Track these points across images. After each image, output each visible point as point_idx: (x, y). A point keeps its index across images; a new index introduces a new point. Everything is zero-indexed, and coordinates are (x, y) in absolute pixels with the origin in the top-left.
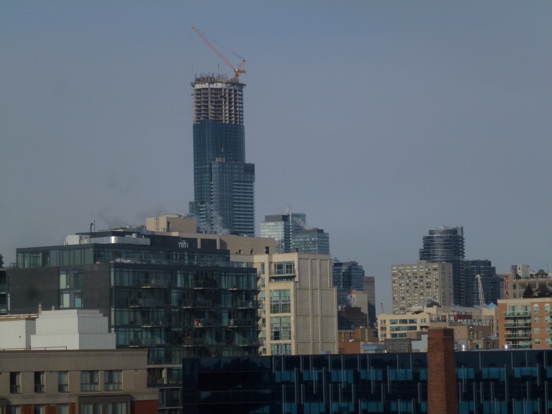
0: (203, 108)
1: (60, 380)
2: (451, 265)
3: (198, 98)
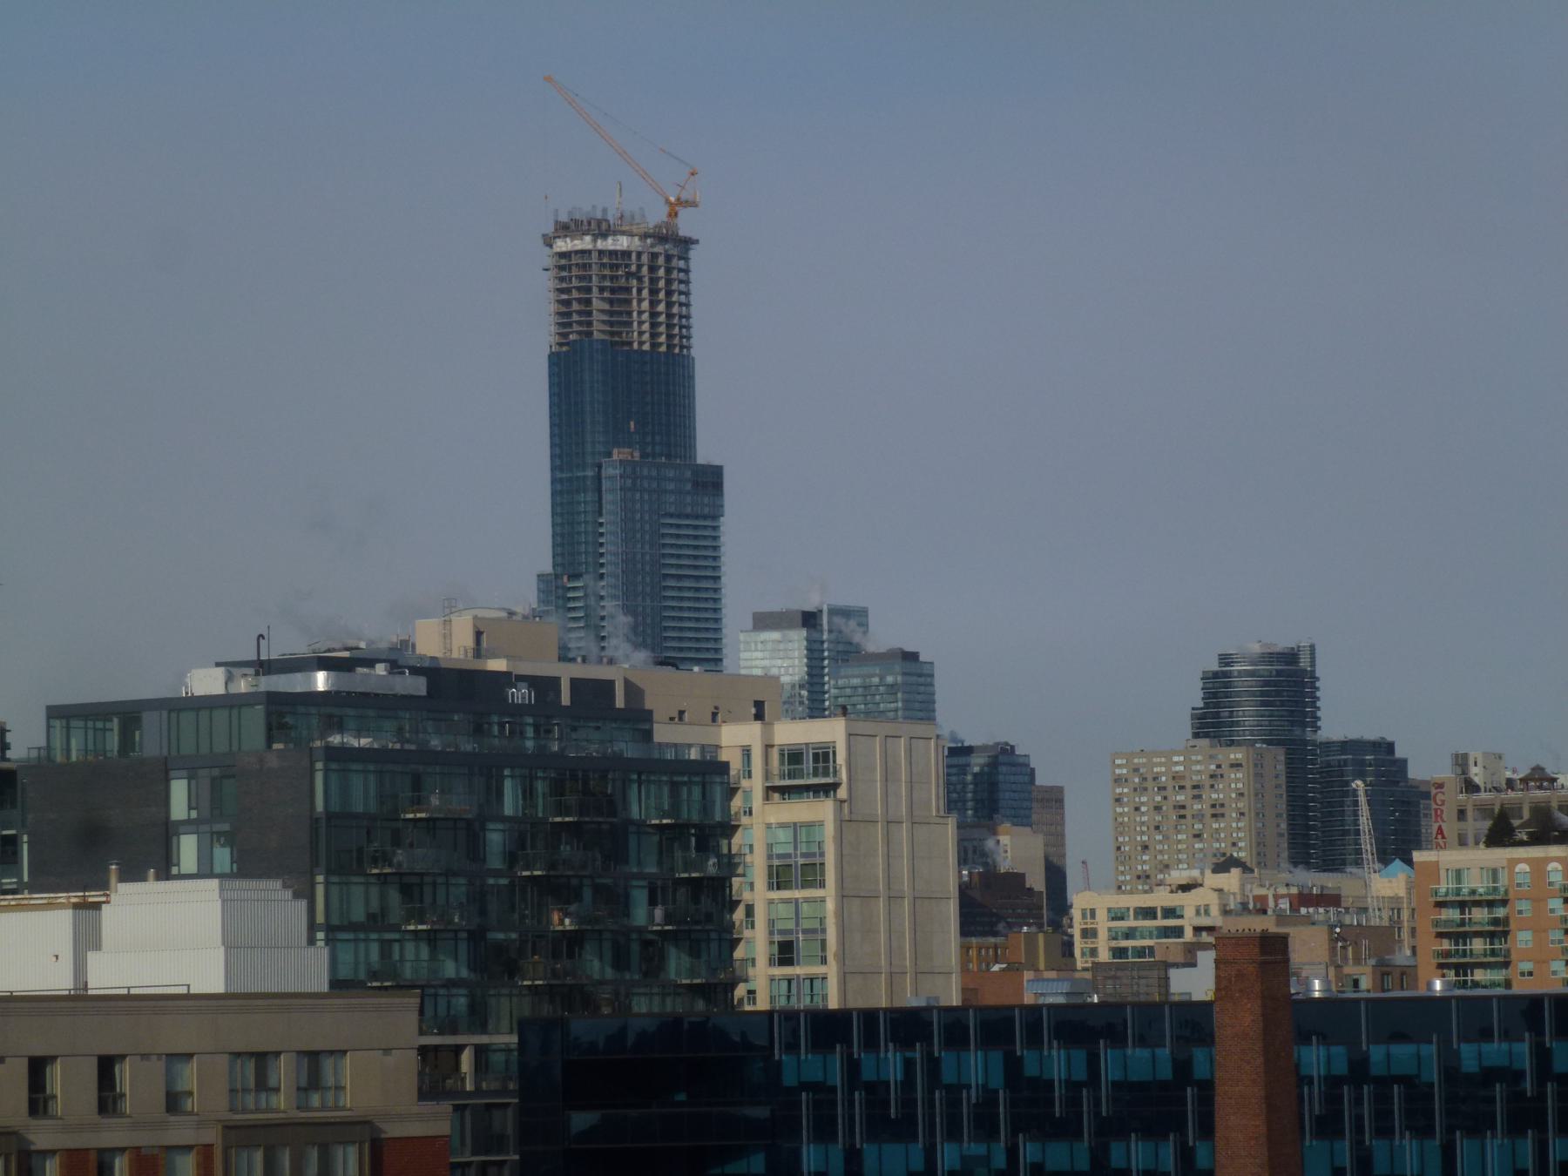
0: (575, 306)
1: (170, 1078)
2: (1280, 754)
3: (562, 279)
